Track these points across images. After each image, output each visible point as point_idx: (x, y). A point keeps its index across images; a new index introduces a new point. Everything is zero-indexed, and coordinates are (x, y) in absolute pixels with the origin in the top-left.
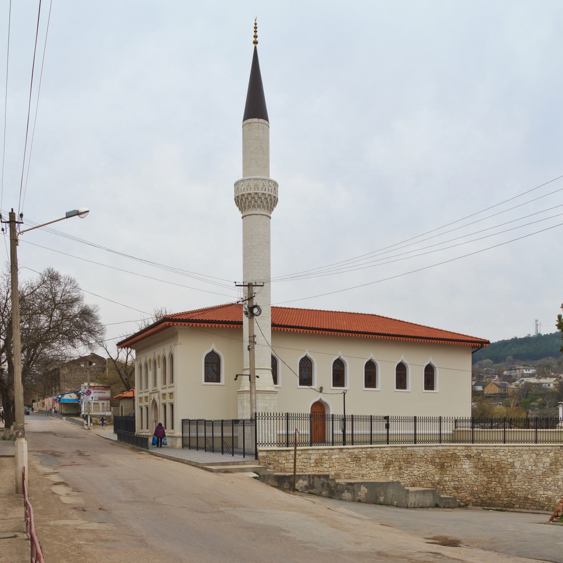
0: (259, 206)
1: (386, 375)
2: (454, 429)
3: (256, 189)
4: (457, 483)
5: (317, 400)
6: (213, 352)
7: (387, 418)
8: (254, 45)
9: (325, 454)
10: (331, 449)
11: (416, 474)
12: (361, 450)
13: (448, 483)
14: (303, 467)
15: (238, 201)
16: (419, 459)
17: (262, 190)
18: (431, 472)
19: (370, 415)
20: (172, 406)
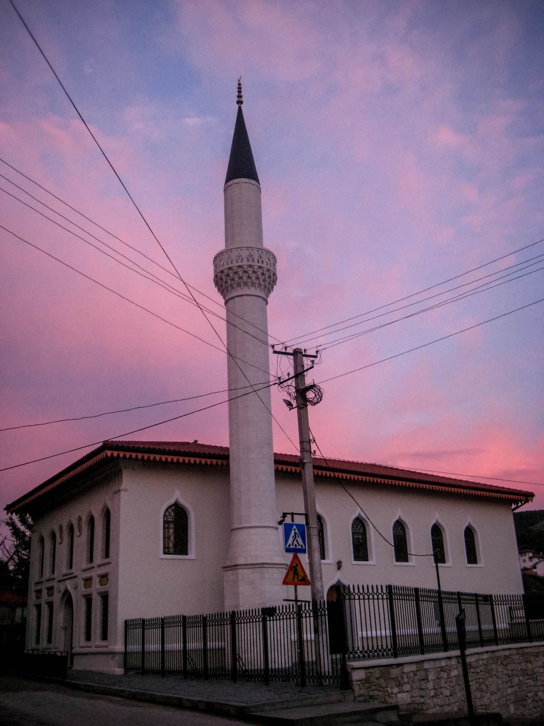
3: (251, 261)
12: (477, 657)
17: (258, 262)
20: (105, 597)
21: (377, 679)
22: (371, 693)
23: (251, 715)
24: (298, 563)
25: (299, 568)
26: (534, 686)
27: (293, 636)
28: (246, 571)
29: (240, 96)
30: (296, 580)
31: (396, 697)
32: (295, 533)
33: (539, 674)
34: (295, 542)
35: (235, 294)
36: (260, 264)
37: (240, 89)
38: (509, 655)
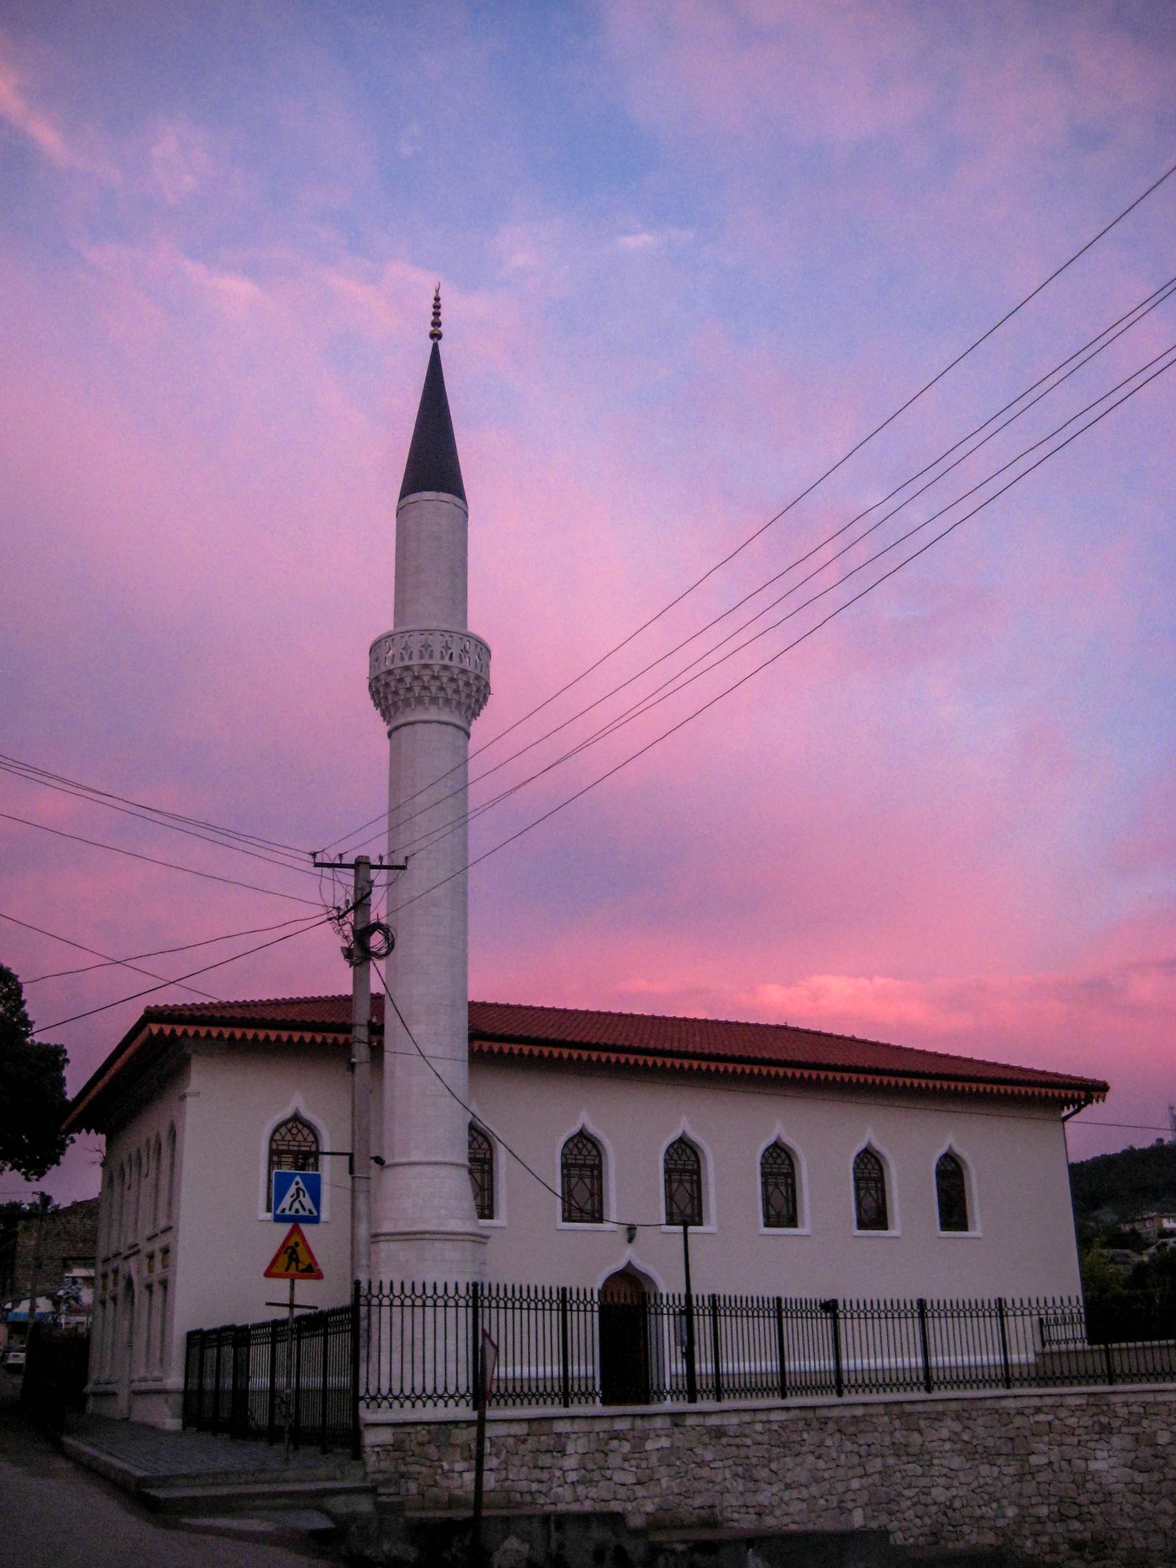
0: (434, 700)
1: (825, 1188)
2: (1039, 1348)
4: (1076, 1525)
5: (619, 1265)
6: (296, 1118)
7: (830, 1307)
8: (431, 342)
9: (617, 1436)
10: (643, 1416)
11: (942, 1499)
12: (747, 1418)
13: (1050, 1527)
14: (535, 1486)
15: (378, 691)
16: (948, 1446)
17: (442, 658)
18: (991, 1489)
19: (772, 1294)
21: (421, 1444)
22: (403, 1469)
23: (148, 1495)
24: (300, 1242)
25: (301, 1250)
26: (923, 1475)
27: (673, 1366)
28: (392, 1246)
29: (436, 324)
30: (293, 1270)
31: (461, 1477)
32: (298, 1190)
33: (937, 1454)
34: (297, 1205)
35: (420, 715)
36: (446, 662)
37: (437, 307)
38: (864, 1416)
